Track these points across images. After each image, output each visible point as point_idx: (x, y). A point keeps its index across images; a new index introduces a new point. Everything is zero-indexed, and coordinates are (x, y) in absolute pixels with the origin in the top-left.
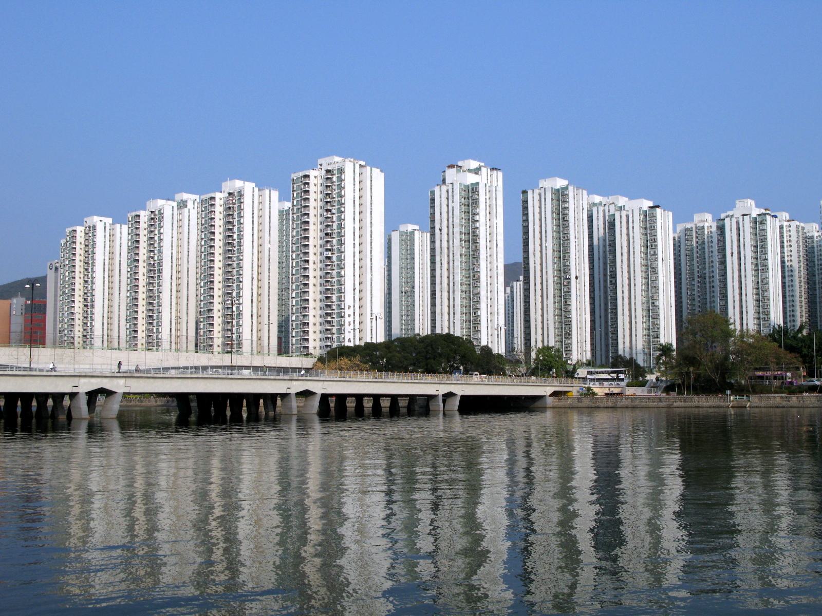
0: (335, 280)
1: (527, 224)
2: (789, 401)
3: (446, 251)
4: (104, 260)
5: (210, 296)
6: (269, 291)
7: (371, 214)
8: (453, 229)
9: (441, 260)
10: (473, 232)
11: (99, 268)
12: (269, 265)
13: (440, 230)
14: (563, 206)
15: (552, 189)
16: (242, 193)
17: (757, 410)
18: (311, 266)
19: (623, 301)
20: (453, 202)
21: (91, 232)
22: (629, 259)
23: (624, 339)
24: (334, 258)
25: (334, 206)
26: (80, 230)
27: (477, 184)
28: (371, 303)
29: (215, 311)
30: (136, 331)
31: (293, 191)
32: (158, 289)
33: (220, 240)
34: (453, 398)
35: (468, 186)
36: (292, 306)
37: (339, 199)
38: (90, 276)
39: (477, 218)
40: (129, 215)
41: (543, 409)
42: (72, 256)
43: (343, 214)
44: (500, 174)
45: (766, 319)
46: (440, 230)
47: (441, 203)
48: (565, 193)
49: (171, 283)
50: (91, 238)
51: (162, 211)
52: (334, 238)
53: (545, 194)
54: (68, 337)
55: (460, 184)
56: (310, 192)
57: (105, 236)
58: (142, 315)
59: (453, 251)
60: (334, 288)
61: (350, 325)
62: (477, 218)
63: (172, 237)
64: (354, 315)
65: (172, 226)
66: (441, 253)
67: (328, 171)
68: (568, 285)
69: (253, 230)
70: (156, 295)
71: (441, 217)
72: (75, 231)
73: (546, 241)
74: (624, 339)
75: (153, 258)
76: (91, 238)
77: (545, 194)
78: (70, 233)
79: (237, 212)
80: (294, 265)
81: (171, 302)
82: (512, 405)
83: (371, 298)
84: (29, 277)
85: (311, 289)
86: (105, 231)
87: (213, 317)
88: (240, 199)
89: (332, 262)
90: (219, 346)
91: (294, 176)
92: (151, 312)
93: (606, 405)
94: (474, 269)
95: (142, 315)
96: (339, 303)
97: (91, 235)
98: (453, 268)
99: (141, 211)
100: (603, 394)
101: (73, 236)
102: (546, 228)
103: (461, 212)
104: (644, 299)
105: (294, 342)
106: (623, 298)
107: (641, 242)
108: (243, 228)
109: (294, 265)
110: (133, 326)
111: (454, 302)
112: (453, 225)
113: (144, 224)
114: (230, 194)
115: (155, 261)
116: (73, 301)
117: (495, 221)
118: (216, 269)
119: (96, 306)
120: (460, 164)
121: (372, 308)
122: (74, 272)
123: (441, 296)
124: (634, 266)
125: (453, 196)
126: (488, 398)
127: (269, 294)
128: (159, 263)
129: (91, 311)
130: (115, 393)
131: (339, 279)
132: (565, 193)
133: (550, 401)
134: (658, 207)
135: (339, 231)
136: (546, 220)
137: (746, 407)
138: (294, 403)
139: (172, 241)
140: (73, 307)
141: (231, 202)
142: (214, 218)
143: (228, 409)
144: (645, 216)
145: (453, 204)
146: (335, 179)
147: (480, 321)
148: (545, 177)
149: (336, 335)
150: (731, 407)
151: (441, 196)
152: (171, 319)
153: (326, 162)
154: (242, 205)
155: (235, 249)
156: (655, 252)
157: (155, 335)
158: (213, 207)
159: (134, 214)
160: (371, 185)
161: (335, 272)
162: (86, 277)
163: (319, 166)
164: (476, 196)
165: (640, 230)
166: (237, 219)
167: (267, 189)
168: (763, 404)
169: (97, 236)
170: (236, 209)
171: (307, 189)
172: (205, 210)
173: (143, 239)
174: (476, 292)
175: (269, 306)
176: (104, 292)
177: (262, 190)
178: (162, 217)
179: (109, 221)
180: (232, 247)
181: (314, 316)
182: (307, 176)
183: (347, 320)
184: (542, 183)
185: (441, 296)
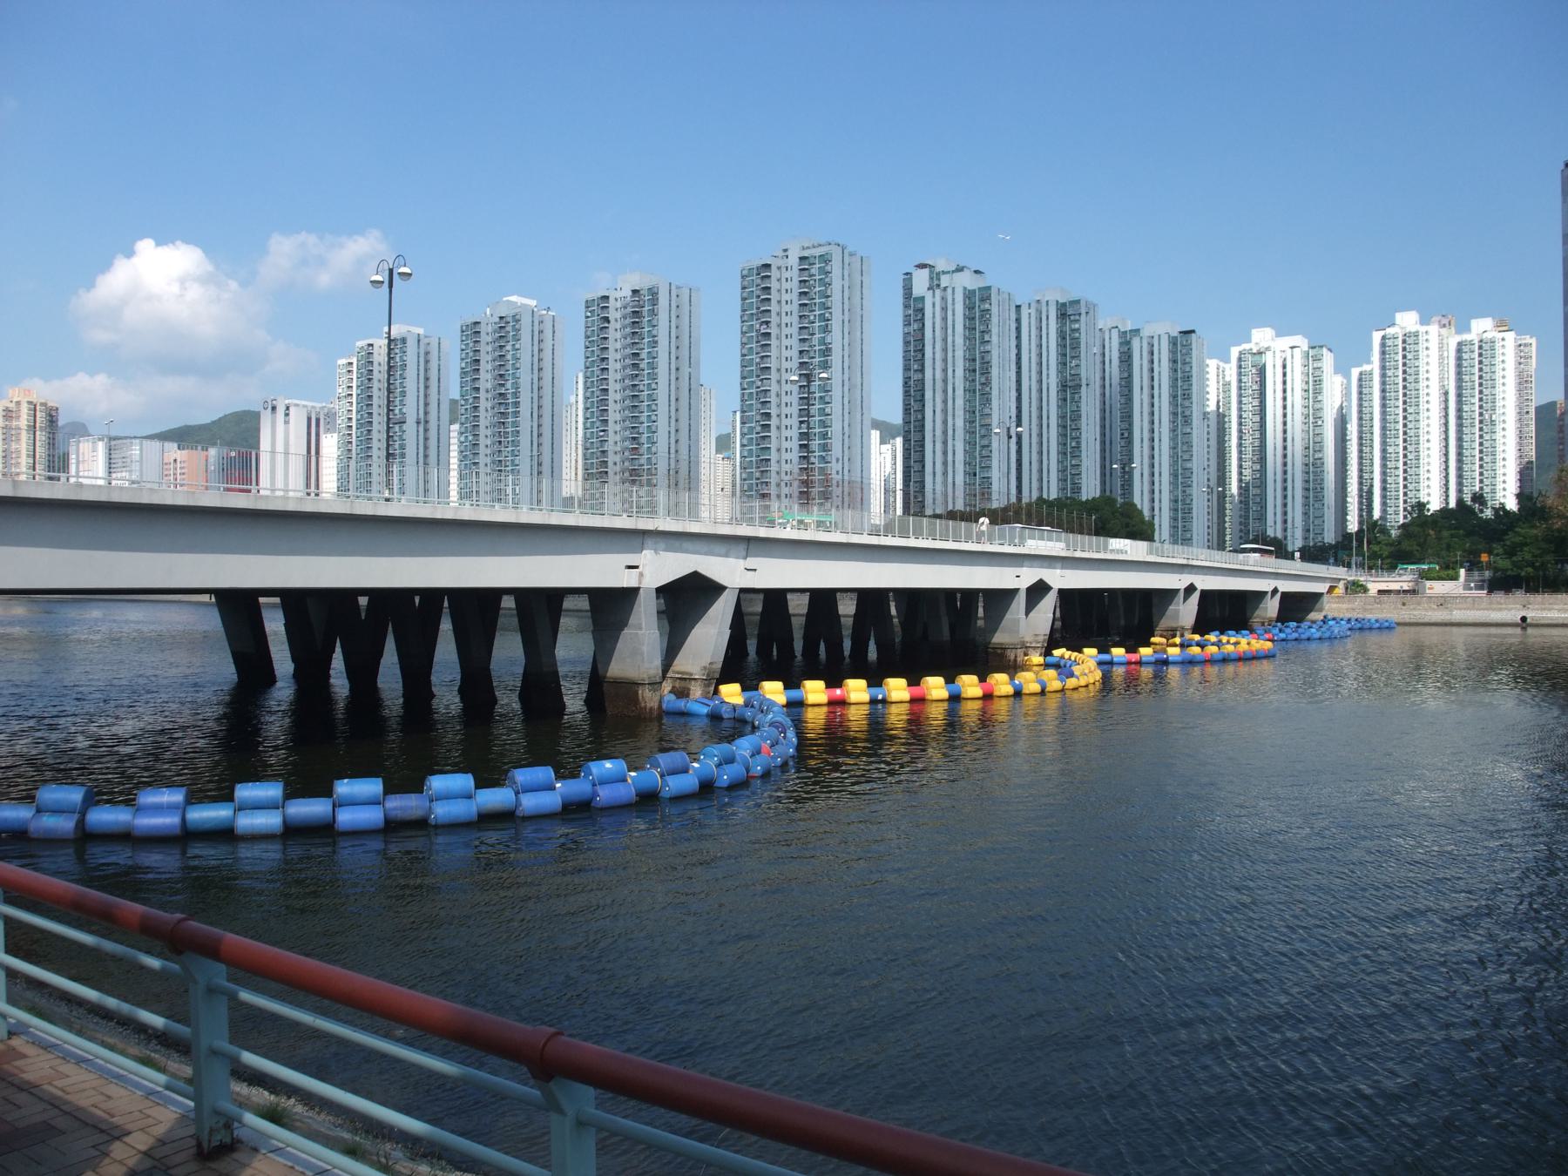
1: (920, 376)
35: (975, 291)
143: (892, 605)
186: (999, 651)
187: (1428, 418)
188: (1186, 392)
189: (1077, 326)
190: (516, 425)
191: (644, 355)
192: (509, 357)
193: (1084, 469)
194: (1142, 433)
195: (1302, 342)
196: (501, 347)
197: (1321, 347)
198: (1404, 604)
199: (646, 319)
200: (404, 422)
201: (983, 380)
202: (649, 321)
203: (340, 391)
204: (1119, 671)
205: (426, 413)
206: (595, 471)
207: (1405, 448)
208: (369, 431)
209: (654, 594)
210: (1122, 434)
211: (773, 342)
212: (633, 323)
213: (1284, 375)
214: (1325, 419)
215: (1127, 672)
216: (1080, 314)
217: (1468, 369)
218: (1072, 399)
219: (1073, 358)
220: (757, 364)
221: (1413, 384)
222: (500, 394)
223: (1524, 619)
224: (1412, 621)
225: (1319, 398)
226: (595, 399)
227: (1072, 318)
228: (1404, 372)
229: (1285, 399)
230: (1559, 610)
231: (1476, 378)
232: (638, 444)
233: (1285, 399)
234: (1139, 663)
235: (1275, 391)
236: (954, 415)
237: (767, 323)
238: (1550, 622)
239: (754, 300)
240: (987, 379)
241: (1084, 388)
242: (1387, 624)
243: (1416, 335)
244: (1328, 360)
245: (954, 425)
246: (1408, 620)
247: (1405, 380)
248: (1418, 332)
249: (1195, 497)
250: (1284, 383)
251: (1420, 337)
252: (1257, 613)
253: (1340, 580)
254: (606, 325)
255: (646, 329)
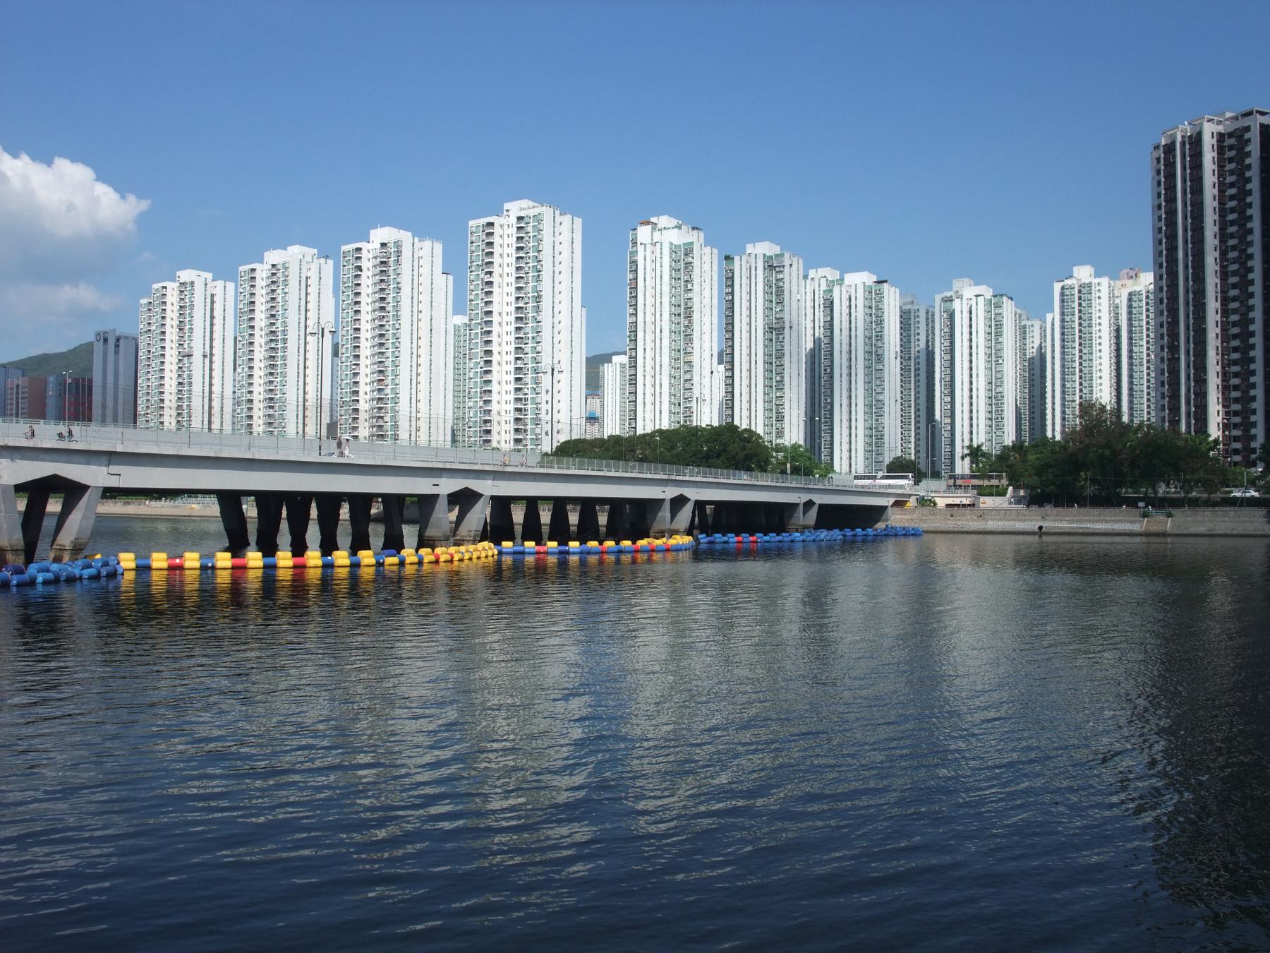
26: (172, 287)
27: (692, 243)
35: (680, 246)
45: (1000, 419)
61: (547, 414)
100: (944, 505)
120: (653, 220)
134: (886, 281)
136: (756, 293)
148: (754, 241)
179: (209, 276)
184: (750, 248)
186: (431, 542)
187: (1100, 358)
188: (998, 323)
189: (781, 276)
190: (285, 359)
191: (390, 299)
192: (279, 299)
193: (786, 400)
194: (841, 369)
195: (988, 292)
196: (273, 291)
197: (1002, 295)
198: (952, 516)
199: (392, 268)
200: (192, 355)
201: (686, 323)
202: (394, 270)
203: (142, 327)
204: (574, 559)
205: (211, 347)
206: (348, 399)
207: (1081, 384)
208: (163, 363)
209: (13, 488)
210: (826, 370)
211: (495, 289)
212: (382, 271)
213: (971, 319)
214: (1005, 358)
215: (537, 560)
216: (784, 266)
217: (1137, 316)
218: (777, 339)
219: (777, 303)
220: (482, 308)
221: (1087, 329)
222: (272, 332)
223: (1041, 528)
224: (956, 529)
225: (1000, 340)
226: (349, 337)
227: (777, 269)
228: (1080, 318)
229: (971, 340)
230: (1069, 521)
231: (1144, 323)
232: (383, 376)
233: (971, 340)
234: (546, 553)
235: (962, 334)
236: (661, 353)
237: (490, 273)
238: (1060, 531)
239: (480, 253)
240: (690, 322)
241: (787, 330)
242: (913, 532)
243: (1090, 285)
244: (1008, 308)
245: (661, 362)
246: (952, 529)
247: (1080, 324)
248: (1091, 283)
249: (886, 425)
250: (971, 326)
251: (1093, 288)
252: (793, 521)
253: (910, 495)
254: (359, 273)
255: (392, 277)
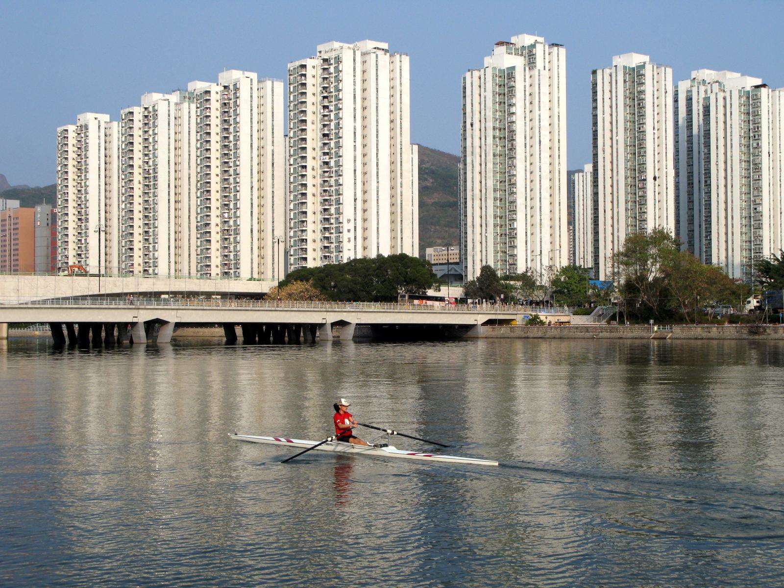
0: (333, 189)
2: (710, 333)
3: (477, 150)
4: (99, 165)
5: (207, 207)
6: (273, 202)
7: (377, 110)
8: (485, 124)
9: (473, 161)
10: (509, 127)
11: (93, 175)
12: (273, 171)
13: (472, 125)
14: (639, 89)
15: (625, 67)
16: (238, 86)
17: (679, 342)
18: (309, 172)
19: (718, 206)
20: (485, 91)
21: (83, 132)
22: (725, 154)
23: (718, 254)
24: (332, 164)
25: (331, 102)
27: (513, 68)
28: (378, 215)
29: (213, 225)
30: (131, 249)
31: (290, 84)
32: (154, 200)
33: (217, 142)
34: (348, 326)
36: (290, 219)
37: (337, 93)
38: (83, 184)
39: (513, 110)
40: (122, 112)
41: (475, 338)
42: (64, 160)
43: (341, 111)
44: (563, 51)
46: (472, 125)
47: (472, 92)
48: (641, 72)
49: (169, 192)
50: (83, 140)
51: (156, 108)
52: (331, 139)
53: (616, 76)
54: (62, 256)
55: (494, 68)
56: (307, 85)
57: (99, 137)
58: (138, 231)
59: (485, 150)
60: (332, 198)
61: (349, 241)
62: (513, 110)
63: (169, 138)
64: (355, 230)
65: (169, 125)
66: (472, 153)
67: (325, 60)
68: (644, 188)
69: (252, 130)
70: (152, 206)
71: (472, 109)
72: (67, 130)
73: (617, 133)
74: (718, 254)
75: (147, 163)
76: (83, 140)
77: (616, 76)
78: (61, 133)
79: (233, 109)
80: (292, 171)
81: (169, 215)
82: (446, 334)
83: (378, 209)
84: (29, 185)
85: (310, 199)
86: (99, 132)
87: (209, 232)
88: (235, 93)
89: (329, 168)
90: (217, 266)
91: (291, 66)
92: (147, 227)
93: (535, 336)
94: (509, 172)
95: (138, 231)
96: (337, 216)
97: (83, 135)
98: (486, 171)
99: (69, 126)
101: (65, 137)
102: (617, 117)
103: (494, 103)
104: (744, 203)
105: (292, 262)
106: (718, 204)
107: (740, 132)
108: (239, 128)
109: (292, 171)
110: (128, 243)
111: (486, 212)
112: (485, 119)
113: (138, 123)
114: (225, 87)
115: (150, 166)
116: (67, 214)
117: (537, 112)
118: (213, 176)
119: (90, 220)
121: (378, 222)
122: (67, 179)
123: (473, 205)
124: (732, 163)
125: (485, 83)
126: (440, 327)
127: (273, 205)
128: (154, 169)
129: (86, 226)
130: (350, 323)
131: (337, 187)
132: (641, 72)
133: (483, 331)
134: (764, 86)
135: (337, 131)
137: (665, 338)
138: (330, 333)
139: (169, 142)
140: (67, 221)
141: (226, 97)
142: (210, 116)
144: (748, 98)
145: (486, 94)
146: (332, 70)
147: (516, 234)
148: (619, 53)
149: (335, 254)
150: (652, 338)
151: (472, 84)
152: (169, 234)
153: (327, 48)
154: (238, 100)
155: (232, 153)
156: (758, 144)
157: (151, 254)
158: (208, 103)
159: (127, 110)
160: (377, 76)
161: (333, 180)
162: (79, 186)
163: (318, 54)
164: (512, 84)
165: (740, 116)
166: (233, 117)
167: (269, 80)
168: (683, 335)
169: (90, 137)
170: (232, 105)
171: (304, 82)
172: (201, 107)
173: (138, 140)
174: (511, 199)
175: (273, 218)
176: (99, 203)
177: (264, 81)
178: (156, 115)
180: (229, 150)
181: (314, 231)
182: (304, 66)
183: (345, 236)
185: (473, 205)
